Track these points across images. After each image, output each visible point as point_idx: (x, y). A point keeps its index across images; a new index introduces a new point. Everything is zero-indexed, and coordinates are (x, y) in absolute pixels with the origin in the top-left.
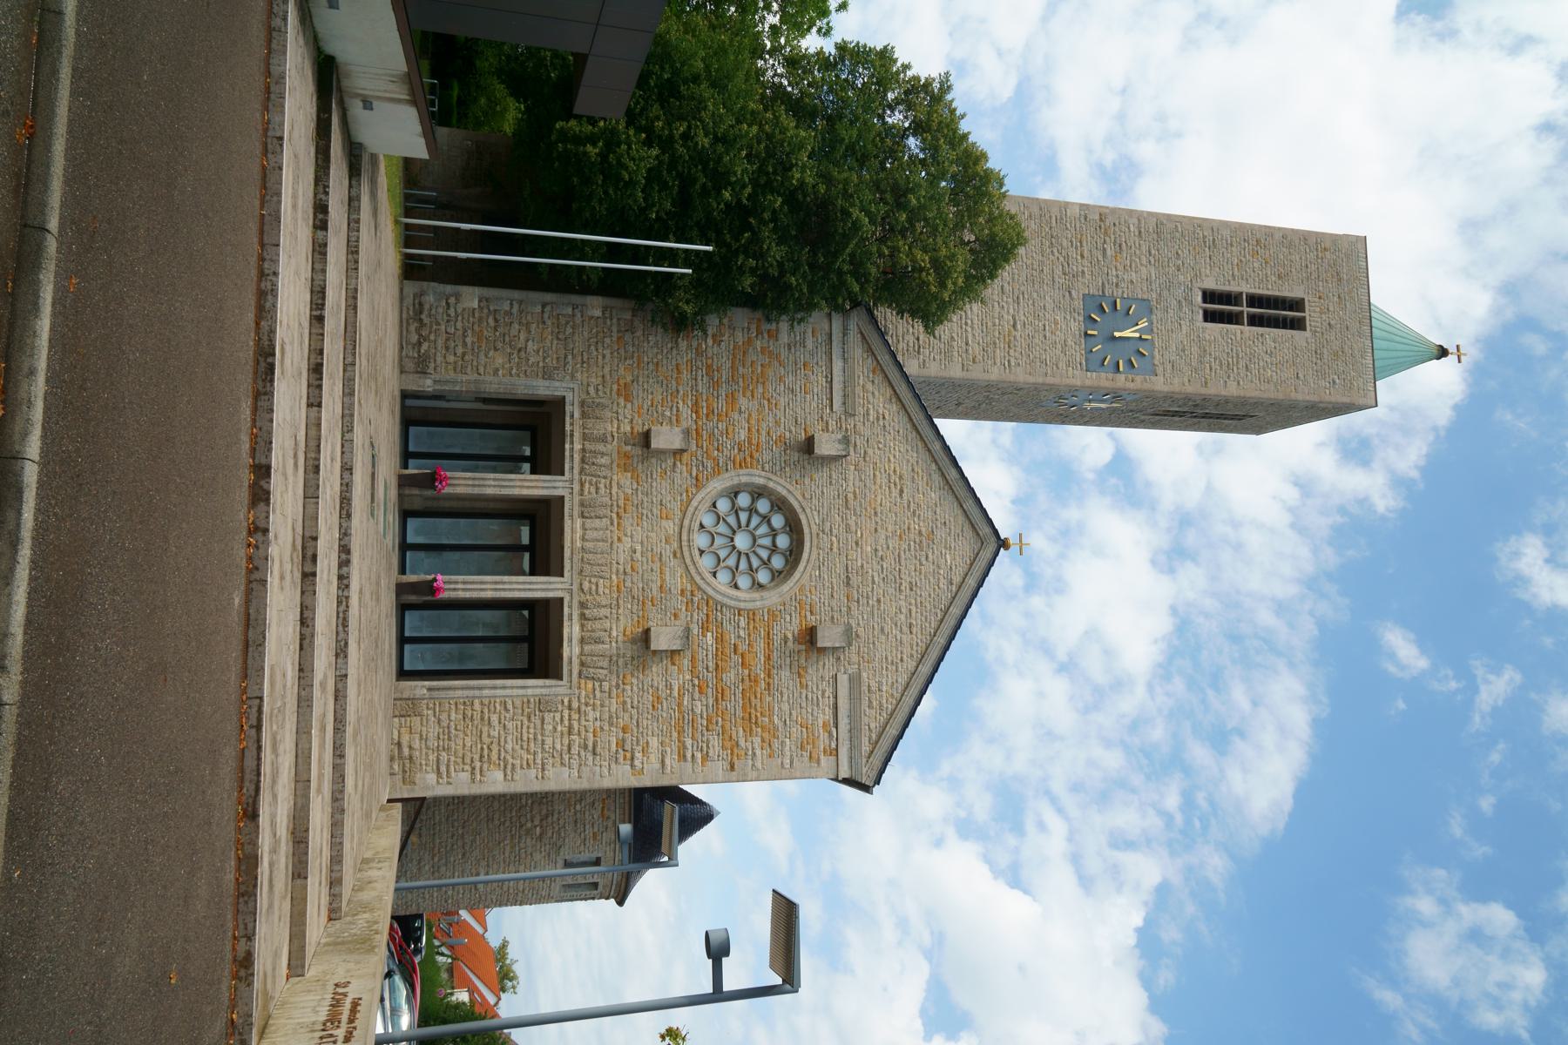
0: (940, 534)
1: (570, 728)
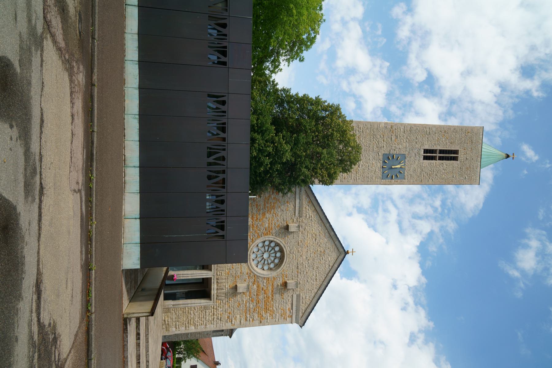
0: (327, 251)
1: (214, 314)
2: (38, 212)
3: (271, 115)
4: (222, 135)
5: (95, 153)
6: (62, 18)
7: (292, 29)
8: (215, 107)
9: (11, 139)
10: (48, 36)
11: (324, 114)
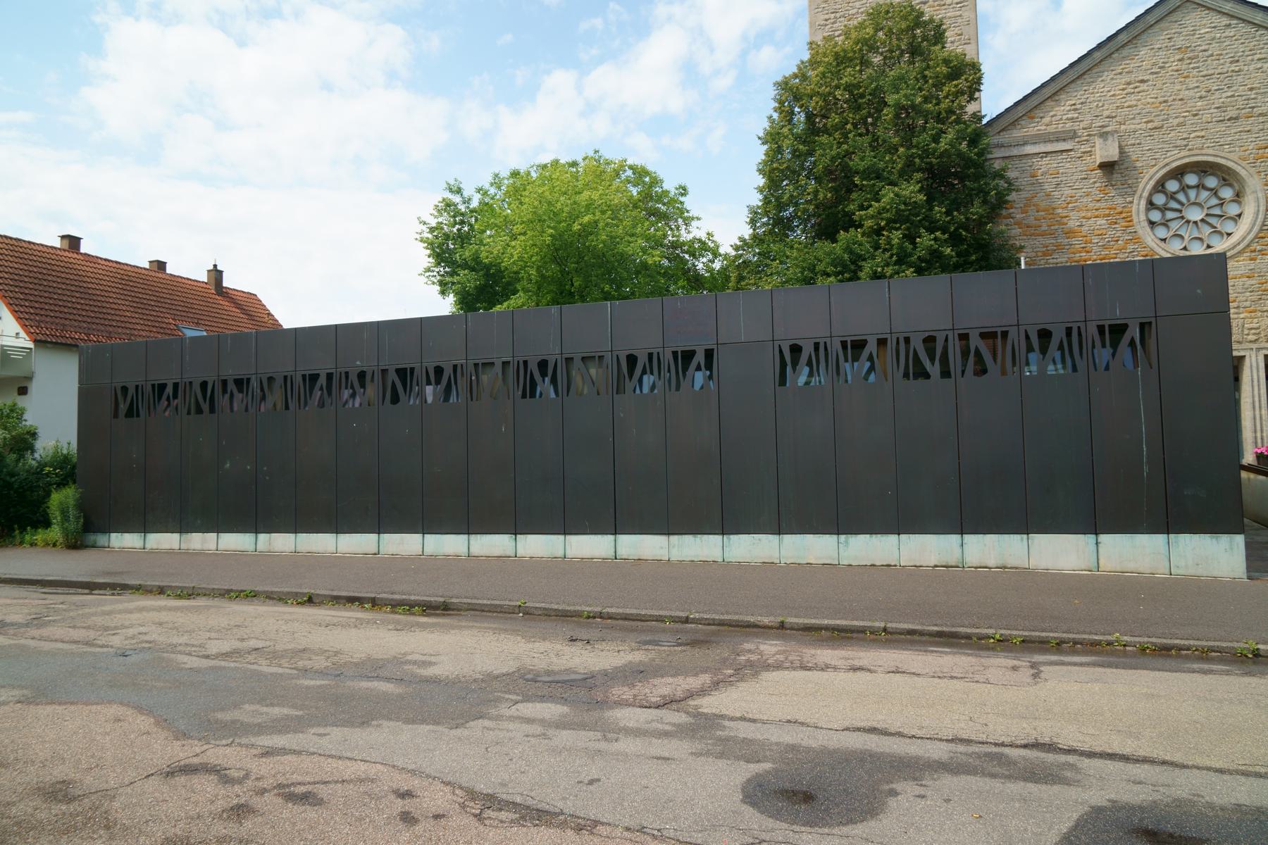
0: (1179, 42)
2: (1101, 761)
3: (812, 244)
4: (872, 347)
5: (936, 628)
6: (655, 676)
7: (621, 220)
8: (806, 370)
9: (923, 797)
10: (692, 703)
11: (800, 117)
